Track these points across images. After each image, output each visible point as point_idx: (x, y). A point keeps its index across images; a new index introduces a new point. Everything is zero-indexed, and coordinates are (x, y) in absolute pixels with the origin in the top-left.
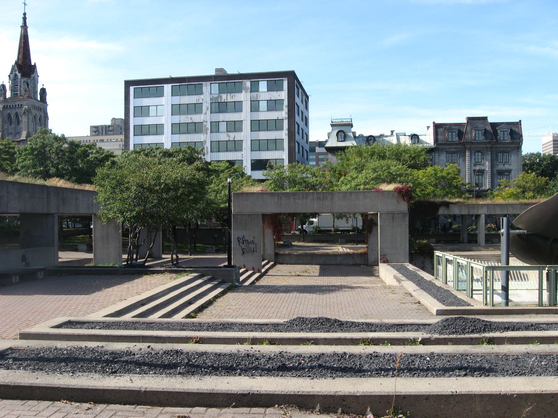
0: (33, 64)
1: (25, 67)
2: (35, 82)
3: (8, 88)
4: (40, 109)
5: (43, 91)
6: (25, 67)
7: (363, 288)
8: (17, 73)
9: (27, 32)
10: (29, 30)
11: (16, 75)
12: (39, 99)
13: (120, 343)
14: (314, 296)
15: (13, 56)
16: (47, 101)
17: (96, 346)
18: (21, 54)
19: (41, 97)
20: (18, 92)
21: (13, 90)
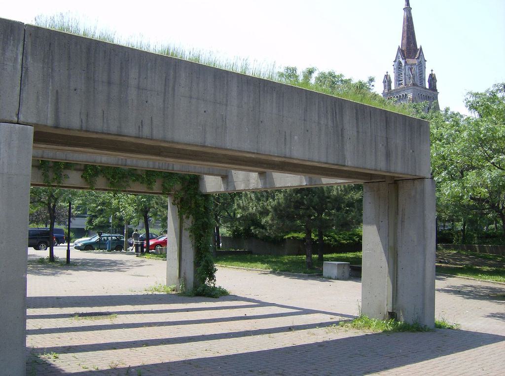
0: (418, 47)
1: (410, 49)
2: (421, 65)
3: (393, 80)
4: (428, 98)
5: (433, 79)
6: (410, 49)
7: (103, 119)
8: (401, 60)
9: (410, 14)
10: (412, 11)
11: (400, 63)
12: (427, 87)
13: (182, 358)
14: (145, 349)
15: (397, 40)
16: (438, 88)
17: (339, 334)
18: (405, 39)
19: (430, 85)
20: (403, 81)
21: (398, 80)
